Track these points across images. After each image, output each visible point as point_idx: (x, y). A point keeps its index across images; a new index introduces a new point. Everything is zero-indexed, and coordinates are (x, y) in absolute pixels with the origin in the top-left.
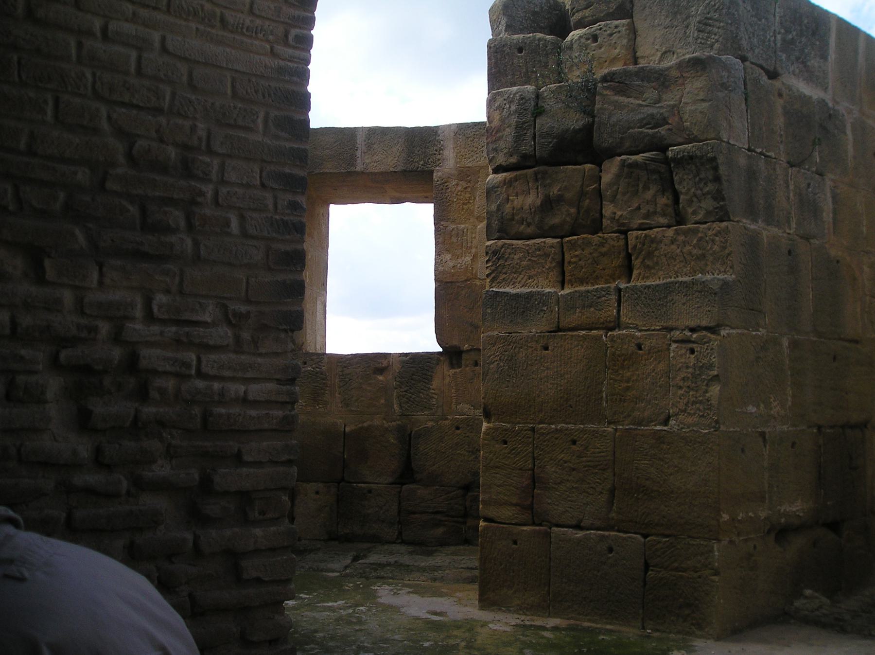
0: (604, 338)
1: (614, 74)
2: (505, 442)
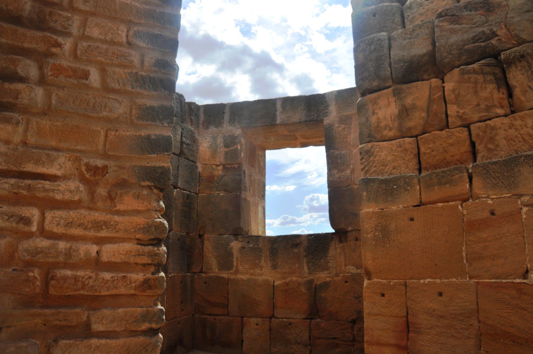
0: (460, 207)
1: (447, 10)
2: (383, 295)
